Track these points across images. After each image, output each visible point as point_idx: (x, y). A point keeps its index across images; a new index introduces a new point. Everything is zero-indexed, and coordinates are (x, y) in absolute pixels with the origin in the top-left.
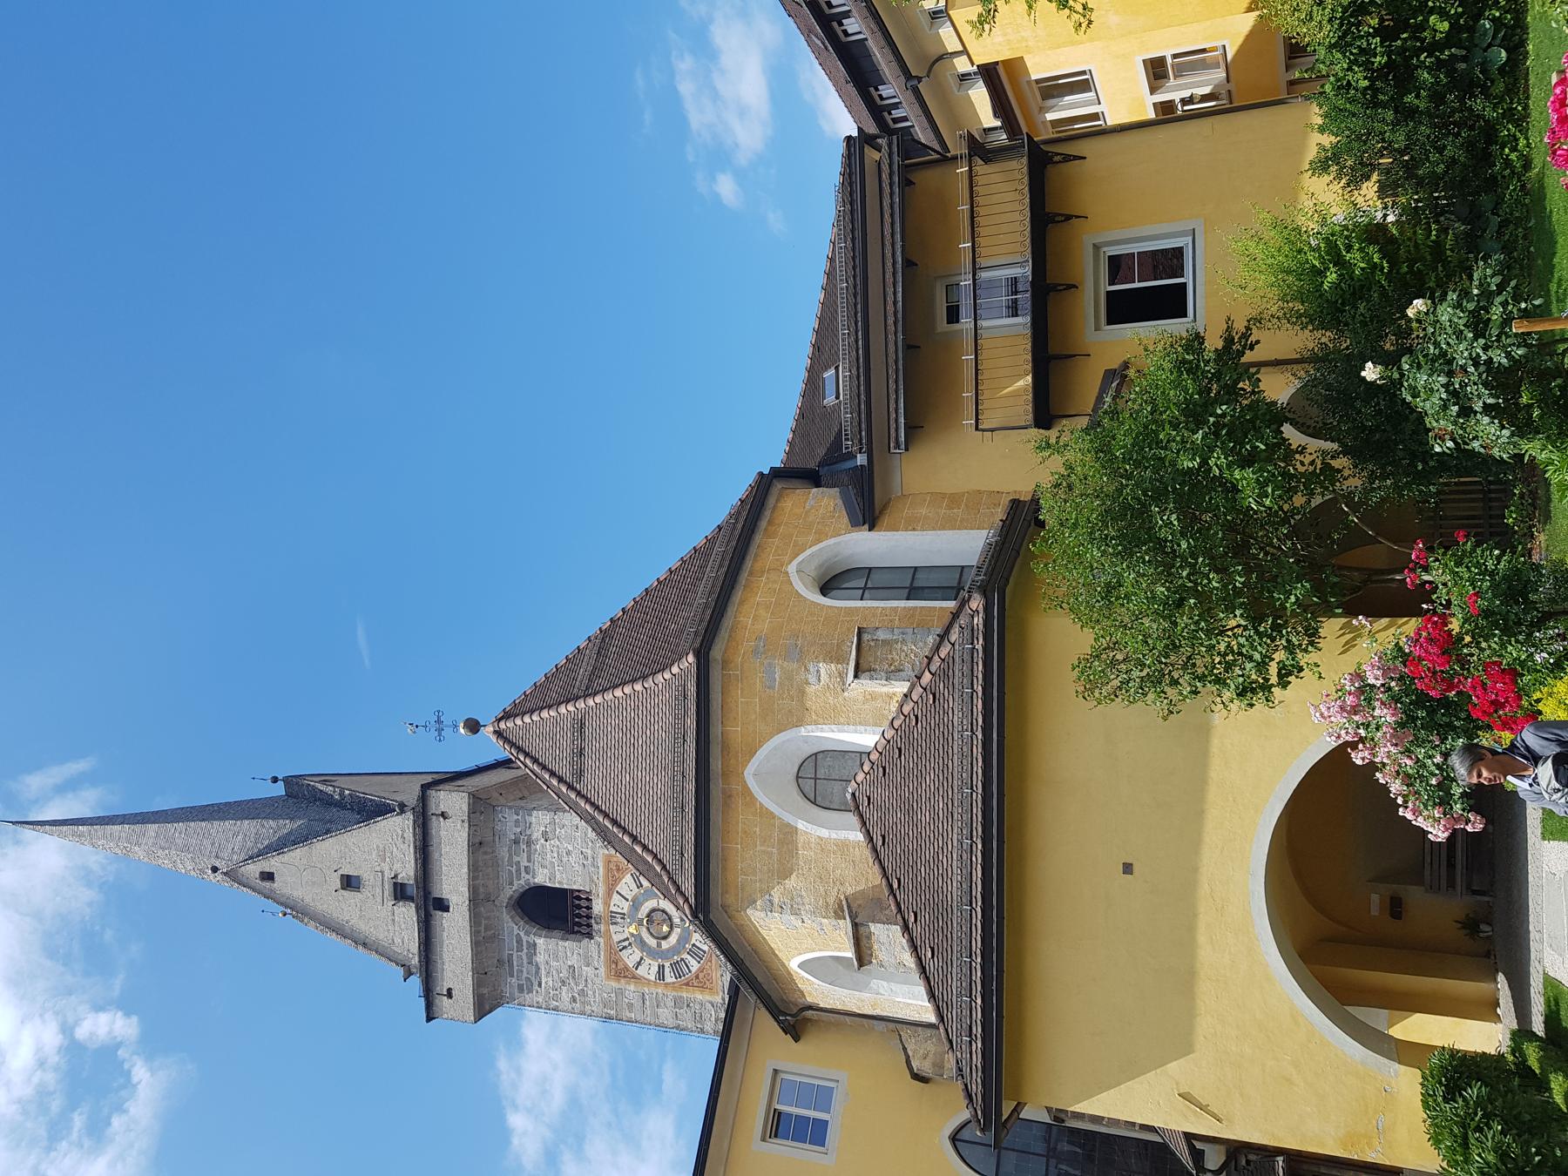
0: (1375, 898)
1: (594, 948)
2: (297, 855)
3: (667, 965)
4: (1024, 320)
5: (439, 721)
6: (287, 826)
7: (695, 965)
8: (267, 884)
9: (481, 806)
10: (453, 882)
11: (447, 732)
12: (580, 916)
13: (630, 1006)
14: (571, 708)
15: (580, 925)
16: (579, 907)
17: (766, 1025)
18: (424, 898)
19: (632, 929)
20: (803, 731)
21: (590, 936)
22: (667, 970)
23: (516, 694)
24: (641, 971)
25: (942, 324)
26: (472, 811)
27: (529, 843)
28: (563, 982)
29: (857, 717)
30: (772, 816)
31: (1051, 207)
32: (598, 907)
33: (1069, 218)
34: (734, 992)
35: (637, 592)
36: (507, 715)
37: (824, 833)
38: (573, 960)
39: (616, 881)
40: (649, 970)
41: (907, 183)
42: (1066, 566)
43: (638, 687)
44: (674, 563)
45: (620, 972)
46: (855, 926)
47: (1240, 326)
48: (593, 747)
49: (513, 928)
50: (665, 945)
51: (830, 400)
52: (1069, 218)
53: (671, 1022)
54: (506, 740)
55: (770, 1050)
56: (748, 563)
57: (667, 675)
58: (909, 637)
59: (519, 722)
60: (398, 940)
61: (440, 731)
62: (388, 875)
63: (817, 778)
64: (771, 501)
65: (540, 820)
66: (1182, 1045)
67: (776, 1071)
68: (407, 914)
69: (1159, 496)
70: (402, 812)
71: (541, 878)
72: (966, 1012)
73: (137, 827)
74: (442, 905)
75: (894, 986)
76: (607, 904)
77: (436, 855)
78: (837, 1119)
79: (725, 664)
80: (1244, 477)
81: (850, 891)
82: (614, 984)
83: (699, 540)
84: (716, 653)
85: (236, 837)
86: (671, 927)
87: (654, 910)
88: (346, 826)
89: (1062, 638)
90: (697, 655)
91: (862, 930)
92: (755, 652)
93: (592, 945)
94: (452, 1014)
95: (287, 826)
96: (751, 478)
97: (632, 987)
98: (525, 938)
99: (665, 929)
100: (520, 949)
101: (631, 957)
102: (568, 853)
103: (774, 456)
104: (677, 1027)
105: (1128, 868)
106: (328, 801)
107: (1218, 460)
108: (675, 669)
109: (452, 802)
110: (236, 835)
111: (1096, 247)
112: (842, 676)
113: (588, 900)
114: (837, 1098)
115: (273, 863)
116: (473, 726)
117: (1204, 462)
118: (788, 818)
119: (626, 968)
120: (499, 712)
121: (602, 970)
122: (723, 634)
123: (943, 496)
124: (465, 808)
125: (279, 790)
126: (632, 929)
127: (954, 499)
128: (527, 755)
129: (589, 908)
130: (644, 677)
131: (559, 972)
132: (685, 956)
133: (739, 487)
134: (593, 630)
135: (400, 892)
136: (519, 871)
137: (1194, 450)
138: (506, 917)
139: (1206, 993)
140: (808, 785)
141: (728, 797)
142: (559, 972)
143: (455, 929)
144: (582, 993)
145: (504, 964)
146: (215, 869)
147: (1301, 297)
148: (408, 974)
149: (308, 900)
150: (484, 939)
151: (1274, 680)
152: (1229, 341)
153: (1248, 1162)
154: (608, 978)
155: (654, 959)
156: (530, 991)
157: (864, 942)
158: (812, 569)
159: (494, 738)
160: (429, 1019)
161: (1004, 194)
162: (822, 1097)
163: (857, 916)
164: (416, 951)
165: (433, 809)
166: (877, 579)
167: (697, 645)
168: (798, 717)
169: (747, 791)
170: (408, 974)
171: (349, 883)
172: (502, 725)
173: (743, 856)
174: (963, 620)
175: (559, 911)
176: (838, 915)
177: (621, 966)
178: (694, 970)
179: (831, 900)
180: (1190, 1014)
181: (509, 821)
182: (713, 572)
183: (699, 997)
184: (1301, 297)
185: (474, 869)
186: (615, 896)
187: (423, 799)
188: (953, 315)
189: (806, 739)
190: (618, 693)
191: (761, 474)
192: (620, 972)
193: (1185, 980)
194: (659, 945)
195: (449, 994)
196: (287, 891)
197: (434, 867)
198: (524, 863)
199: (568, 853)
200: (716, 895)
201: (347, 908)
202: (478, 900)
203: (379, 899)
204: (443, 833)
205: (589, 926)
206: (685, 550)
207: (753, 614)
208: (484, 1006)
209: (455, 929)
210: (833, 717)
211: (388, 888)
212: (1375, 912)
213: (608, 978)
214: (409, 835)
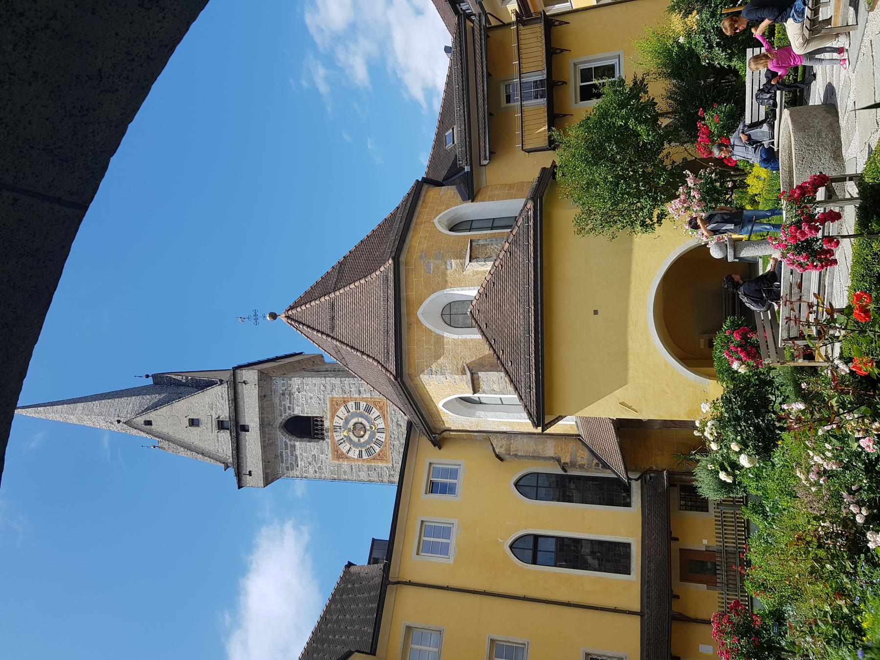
0: (702, 341)
1: (326, 445)
2: (164, 410)
3: (363, 450)
4: (543, 101)
5: (255, 315)
6: (156, 397)
7: (377, 449)
8: (148, 427)
9: (264, 378)
10: (251, 416)
11: (260, 320)
12: (317, 430)
13: (345, 472)
14: (327, 298)
15: (317, 434)
16: (317, 425)
17: (424, 443)
18: (235, 427)
19: (345, 433)
21: (323, 439)
23: (296, 298)
24: (350, 454)
25: (504, 103)
26: (260, 380)
27: (290, 394)
29: (468, 281)
31: (554, 45)
32: (327, 424)
33: (562, 50)
34: (410, 425)
35: (357, 242)
36: (291, 308)
37: (456, 337)
38: (315, 452)
39: (336, 410)
40: (354, 453)
41: (487, 37)
42: (567, 185)
43: (363, 281)
44: (375, 227)
45: (339, 455)
46: (472, 374)
47: (640, 77)
48: (339, 314)
49: (283, 438)
50: (362, 440)
51: (449, 146)
52: (562, 50)
53: (366, 479)
54: (292, 319)
55: (428, 455)
56: (414, 219)
57: (378, 273)
58: (494, 242)
59: (299, 309)
61: (256, 319)
62: (215, 417)
63: (452, 314)
64: (423, 193)
65: (296, 382)
66: (622, 381)
67: (430, 464)
68: (225, 437)
69: (608, 139)
70: (221, 384)
71: (298, 412)
72: (527, 380)
73: (72, 406)
74: (245, 429)
75: (487, 413)
76: (332, 422)
77: (241, 403)
78: (460, 483)
79: (407, 263)
80: (641, 128)
81: (468, 362)
82: (337, 462)
83: (387, 215)
84: (402, 259)
85: (128, 406)
86: (365, 432)
88: (190, 394)
89: (566, 213)
90: (394, 259)
91: (475, 376)
92: (421, 257)
94: (252, 484)
95: (156, 397)
96: (412, 183)
98: (289, 443)
99: (362, 433)
100: (286, 449)
101: (344, 448)
102: (311, 398)
103: (421, 175)
104: (370, 481)
105: (596, 312)
106: (179, 384)
107: (631, 123)
108: (382, 269)
109: (250, 376)
110: (128, 404)
111: (575, 65)
112: (463, 265)
113: (322, 421)
115: (151, 416)
116: (274, 316)
117: (626, 124)
119: (342, 454)
120: (287, 307)
121: (330, 456)
122: (405, 250)
123: (506, 185)
124: (256, 378)
125: (150, 381)
126: (345, 433)
127: (511, 187)
128: (304, 324)
129: (322, 425)
130: (366, 277)
131: (307, 458)
132: (373, 445)
133: (407, 187)
134: (334, 263)
135: (221, 425)
136: (285, 409)
137: (622, 118)
139: (631, 358)
140: (447, 318)
141: (409, 325)
142: (307, 458)
143: (252, 442)
144: (320, 468)
145: (279, 457)
146: (119, 422)
147: (665, 65)
148: (227, 467)
149: (170, 434)
150: (267, 445)
151: (655, 219)
152: (635, 83)
153: (651, 478)
154: (333, 459)
156: (292, 469)
157: (476, 382)
158: (445, 221)
159: (285, 320)
160: (240, 487)
161: (533, 39)
162: (454, 473)
163: (473, 372)
164: (230, 455)
165: (239, 379)
166: (475, 225)
167: (393, 254)
168: (444, 285)
169: (419, 321)
170: (227, 467)
171: (193, 423)
172: (290, 312)
173: (417, 350)
174: (524, 213)
175: (306, 428)
176: (463, 373)
177: (339, 452)
179: (460, 367)
180: (626, 369)
181: (279, 384)
182: (398, 226)
183: (380, 464)
184: (665, 65)
185: (262, 408)
186: (336, 418)
187: (234, 375)
188: (508, 100)
189: (446, 295)
190: (352, 286)
191: (417, 181)
192: (339, 455)
193: (624, 354)
195: (250, 474)
196: (159, 430)
197: (241, 409)
198: (288, 405)
199: (311, 398)
200: (405, 370)
201: (193, 436)
202: (264, 425)
203: (210, 430)
204: (245, 392)
205: (323, 434)
206: (380, 220)
207: (418, 241)
208: (268, 479)
209: (252, 442)
210: (459, 284)
211: (215, 424)
212: (702, 347)
213: (333, 459)
214: (225, 395)
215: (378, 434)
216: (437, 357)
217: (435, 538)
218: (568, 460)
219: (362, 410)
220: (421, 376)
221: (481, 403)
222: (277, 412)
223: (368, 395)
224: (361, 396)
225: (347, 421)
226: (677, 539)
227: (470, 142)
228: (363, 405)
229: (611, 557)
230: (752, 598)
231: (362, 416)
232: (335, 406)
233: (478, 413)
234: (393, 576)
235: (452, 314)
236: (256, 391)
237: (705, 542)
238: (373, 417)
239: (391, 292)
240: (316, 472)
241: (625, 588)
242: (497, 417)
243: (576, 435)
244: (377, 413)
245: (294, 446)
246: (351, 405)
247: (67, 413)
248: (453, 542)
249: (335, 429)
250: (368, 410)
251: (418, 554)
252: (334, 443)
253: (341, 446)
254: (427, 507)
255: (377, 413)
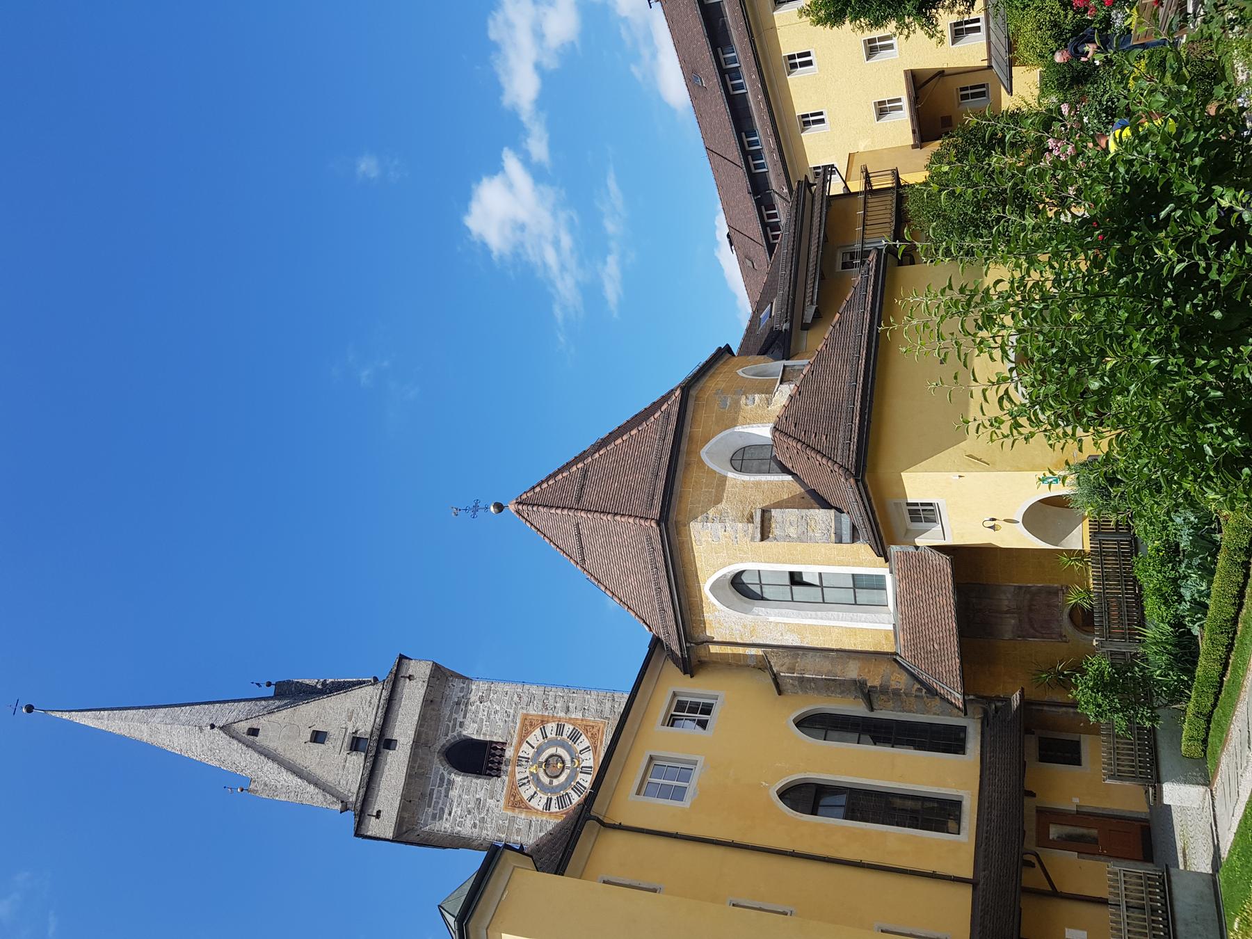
1: (500, 785)
3: (554, 798)
6: (277, 703)
10: (404, 730)
11: (480, 512)
12: (493, 762)
15: (491, 769)
16: (494, 755)
20: (738, 429)
22: (553, 802)
24: (533, 803)
26: (432, 676)
28: (469, 812)
30: (715, 472)
32: (509, 753)
38: (480, 795)
39: (528, 733)
40: (539, 803)
41: (828, 206)
45: (516, 803)
49: (439, 767)
50: (556, 782)
55: (674, 684)
60: (343, 782)
62: (350, 731)
63: (744, 459)
68: (357, 762)
76: (517, 751)
79: (697, 399)
82: (510, 813)
84: (693, 393)
87: (552, 756)
93: (496, 782)
97: (523, 816)
100: (441, 785)
101: (526, 792)
102: (496, 712)
114: (715, 711)
116: (500, 507)
118: (723, 472)
119: (522, 800)
121: (502, 802)
124: (428, 672)
129: (501, 756)
131: (467, 803)
135: (356, 744)
136: (454, 725)
138: (436, 760)
141: (688, 465)
142: (467, 803)
143: (396, 765)
146: (213, 726)
148: (345, 809)
149: (280, 750)
150: (416, 774)
155: (545, 793)
171: (318, 737)
173: (692, 490)
177: (518, 798)
178: (574, 802)
179: (746, 513)
185: (423, 718)
186: (525, 745)
189: (741, 434)
190: (619, 441)
192: (516, 803)
194: (551, 783)
195: (378, 816)
196: (265, 743)
199: (496, 712)
200: (672, 515)
201: (311, 757)
204: (406, 691)
205: (499, 770)
209: (396, 765)
211: (347, 740)
215: (581, 776)
216: (718, 501)
217: (669, 779)
218: (877, 683)
219: (565, 736)
220: (692, 524)
221: (763, 599)
222: (443, 729)
223: (579, 716)
224: (569, 715)
225: (539, 751)
226: (1032, 794)
227: (795, 282)
228: (568, 728)
229: (934, 813)
230: (1136, 540)
231: (563, 745)
232: (528, 725)
233: (756, 609)
234: (596, 809)
235: (744, 459)
236: (423, 692)
237: (1076, 800)
238: (579, 749)
239: (661, 484)
240: (475, 826)
241: (955, 850)
242: (782, 615)
243: (892, 654)
244: (586, 743)
245: (451, 783)
246: (551, 728)
247: (138, 721)
248: (692, 786)
249: (519, 761)
250: (574, 737)
251: (638, 793)
252: (512, 783)
253: (522, 789)
254: (659, 739)
255: (586, 743)
